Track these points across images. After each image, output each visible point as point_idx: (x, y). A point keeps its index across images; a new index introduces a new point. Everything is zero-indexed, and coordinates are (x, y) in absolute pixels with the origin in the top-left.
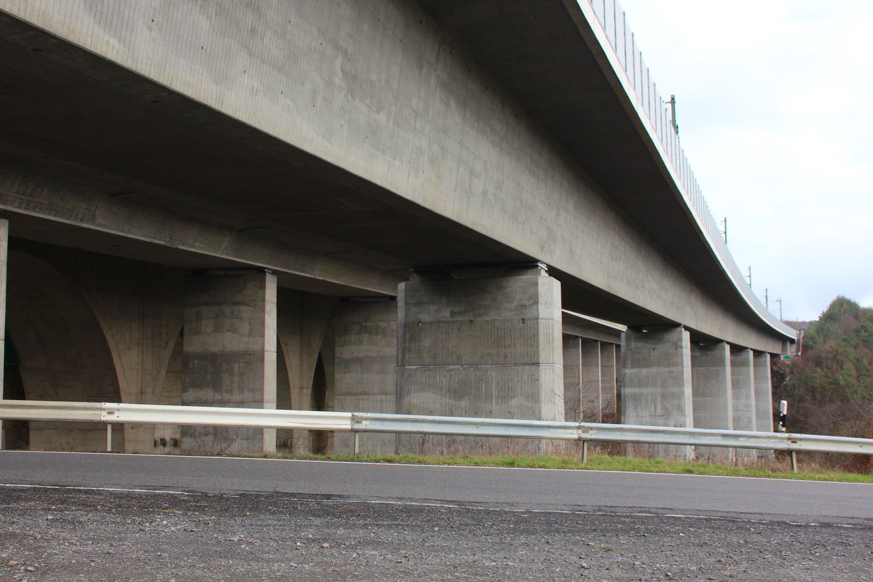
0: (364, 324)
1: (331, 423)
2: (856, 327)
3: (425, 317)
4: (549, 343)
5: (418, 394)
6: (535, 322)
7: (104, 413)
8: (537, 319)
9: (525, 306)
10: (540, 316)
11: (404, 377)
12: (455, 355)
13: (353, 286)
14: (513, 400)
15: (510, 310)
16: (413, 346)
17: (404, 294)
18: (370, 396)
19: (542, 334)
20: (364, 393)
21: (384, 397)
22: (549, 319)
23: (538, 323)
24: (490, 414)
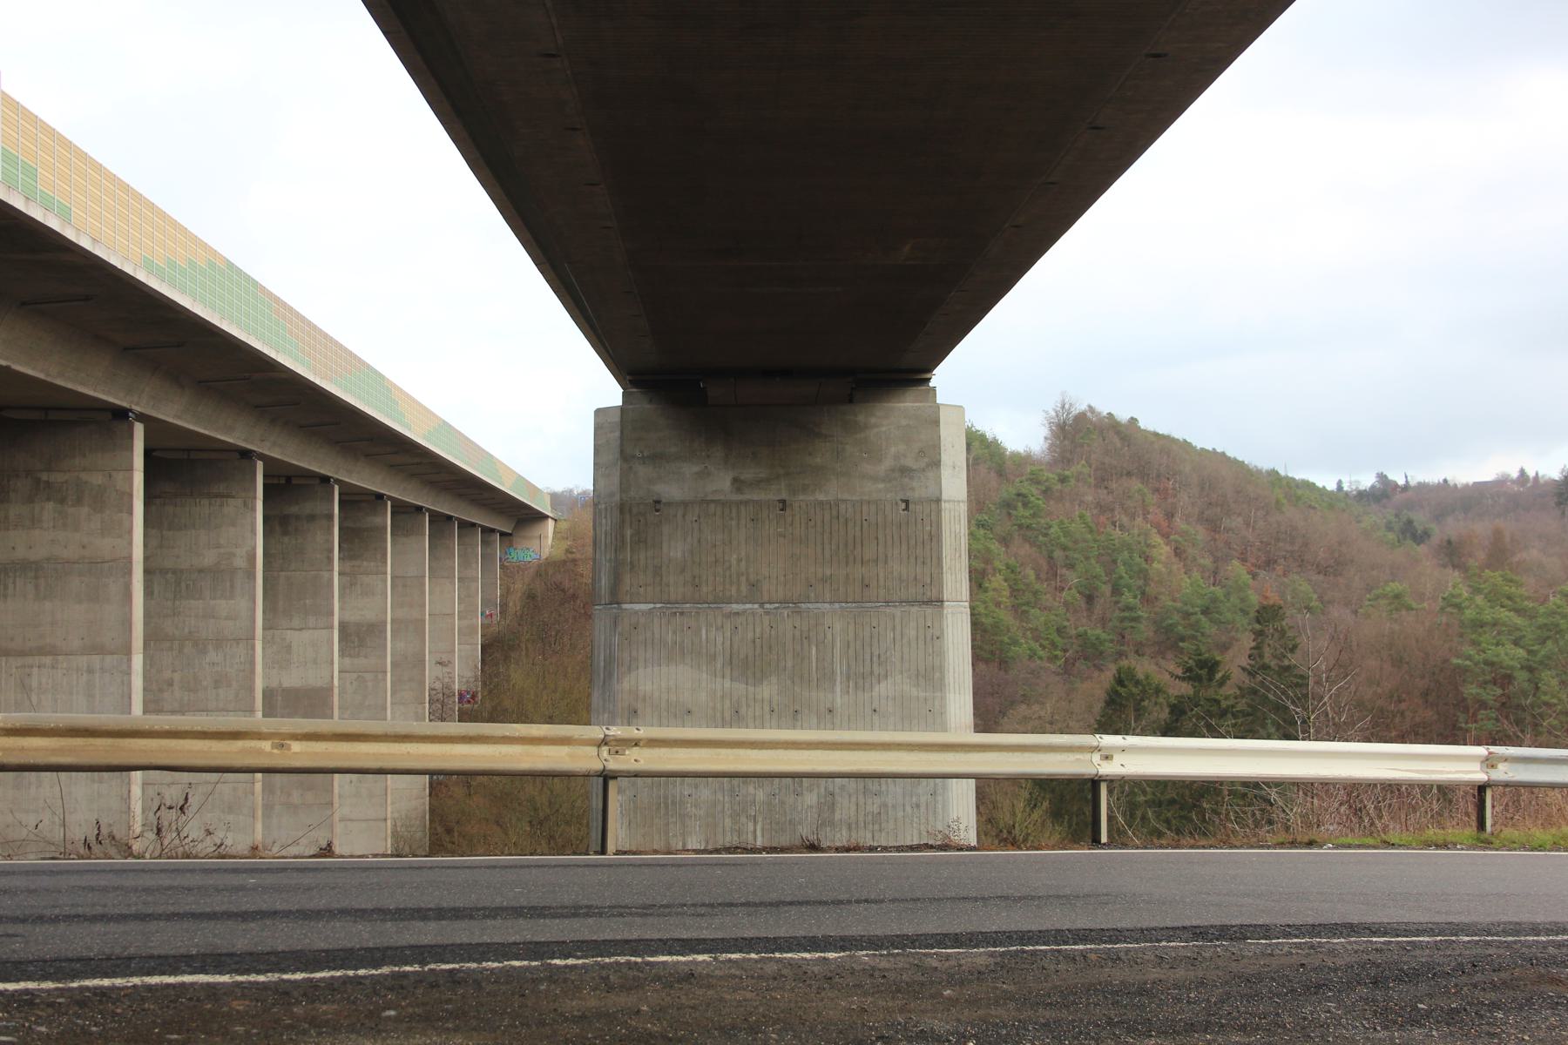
0: (44, 476)
1: (1453, 770)
2: (1005, 495)
3: (671, 491)
4: (960, 556)
5: (656, 669)
6: (934, 506)
7: (1096, 757)
8: (938, 501)
9: (911, 470)
10: (945, 496)
11: (619, 629)
12: (743, 579)
13: (60, 382)
14: (883, 685)
15: (875, 479)
16: (642, 556)
17: (617, 434)
18: (60, 658)
19: (948, 534)
20: (41, 651)
21: (96, 659)
22: (959, 501)
23: (939, 511)
24: (829, 716)
